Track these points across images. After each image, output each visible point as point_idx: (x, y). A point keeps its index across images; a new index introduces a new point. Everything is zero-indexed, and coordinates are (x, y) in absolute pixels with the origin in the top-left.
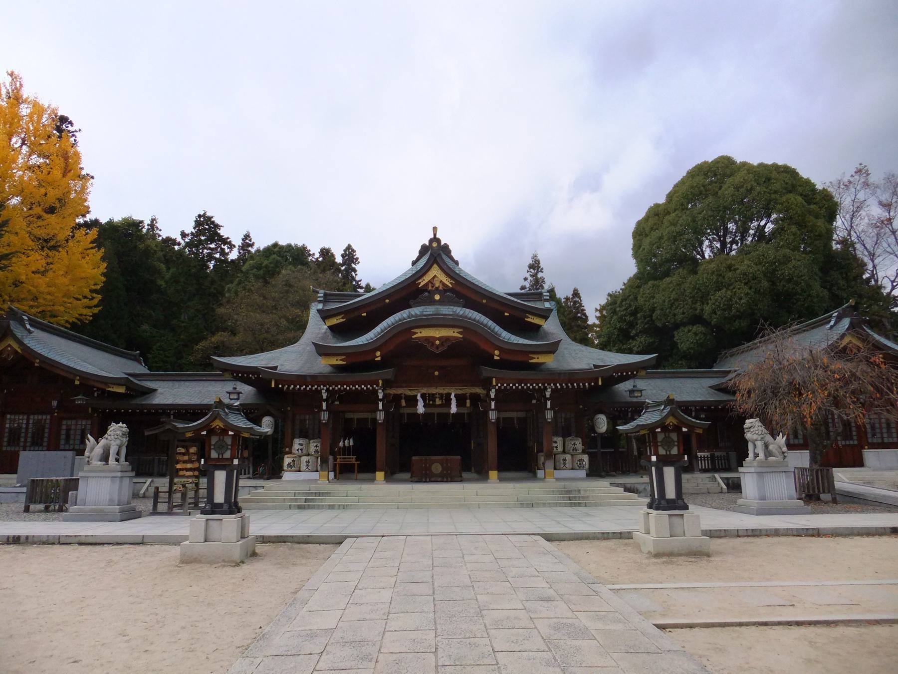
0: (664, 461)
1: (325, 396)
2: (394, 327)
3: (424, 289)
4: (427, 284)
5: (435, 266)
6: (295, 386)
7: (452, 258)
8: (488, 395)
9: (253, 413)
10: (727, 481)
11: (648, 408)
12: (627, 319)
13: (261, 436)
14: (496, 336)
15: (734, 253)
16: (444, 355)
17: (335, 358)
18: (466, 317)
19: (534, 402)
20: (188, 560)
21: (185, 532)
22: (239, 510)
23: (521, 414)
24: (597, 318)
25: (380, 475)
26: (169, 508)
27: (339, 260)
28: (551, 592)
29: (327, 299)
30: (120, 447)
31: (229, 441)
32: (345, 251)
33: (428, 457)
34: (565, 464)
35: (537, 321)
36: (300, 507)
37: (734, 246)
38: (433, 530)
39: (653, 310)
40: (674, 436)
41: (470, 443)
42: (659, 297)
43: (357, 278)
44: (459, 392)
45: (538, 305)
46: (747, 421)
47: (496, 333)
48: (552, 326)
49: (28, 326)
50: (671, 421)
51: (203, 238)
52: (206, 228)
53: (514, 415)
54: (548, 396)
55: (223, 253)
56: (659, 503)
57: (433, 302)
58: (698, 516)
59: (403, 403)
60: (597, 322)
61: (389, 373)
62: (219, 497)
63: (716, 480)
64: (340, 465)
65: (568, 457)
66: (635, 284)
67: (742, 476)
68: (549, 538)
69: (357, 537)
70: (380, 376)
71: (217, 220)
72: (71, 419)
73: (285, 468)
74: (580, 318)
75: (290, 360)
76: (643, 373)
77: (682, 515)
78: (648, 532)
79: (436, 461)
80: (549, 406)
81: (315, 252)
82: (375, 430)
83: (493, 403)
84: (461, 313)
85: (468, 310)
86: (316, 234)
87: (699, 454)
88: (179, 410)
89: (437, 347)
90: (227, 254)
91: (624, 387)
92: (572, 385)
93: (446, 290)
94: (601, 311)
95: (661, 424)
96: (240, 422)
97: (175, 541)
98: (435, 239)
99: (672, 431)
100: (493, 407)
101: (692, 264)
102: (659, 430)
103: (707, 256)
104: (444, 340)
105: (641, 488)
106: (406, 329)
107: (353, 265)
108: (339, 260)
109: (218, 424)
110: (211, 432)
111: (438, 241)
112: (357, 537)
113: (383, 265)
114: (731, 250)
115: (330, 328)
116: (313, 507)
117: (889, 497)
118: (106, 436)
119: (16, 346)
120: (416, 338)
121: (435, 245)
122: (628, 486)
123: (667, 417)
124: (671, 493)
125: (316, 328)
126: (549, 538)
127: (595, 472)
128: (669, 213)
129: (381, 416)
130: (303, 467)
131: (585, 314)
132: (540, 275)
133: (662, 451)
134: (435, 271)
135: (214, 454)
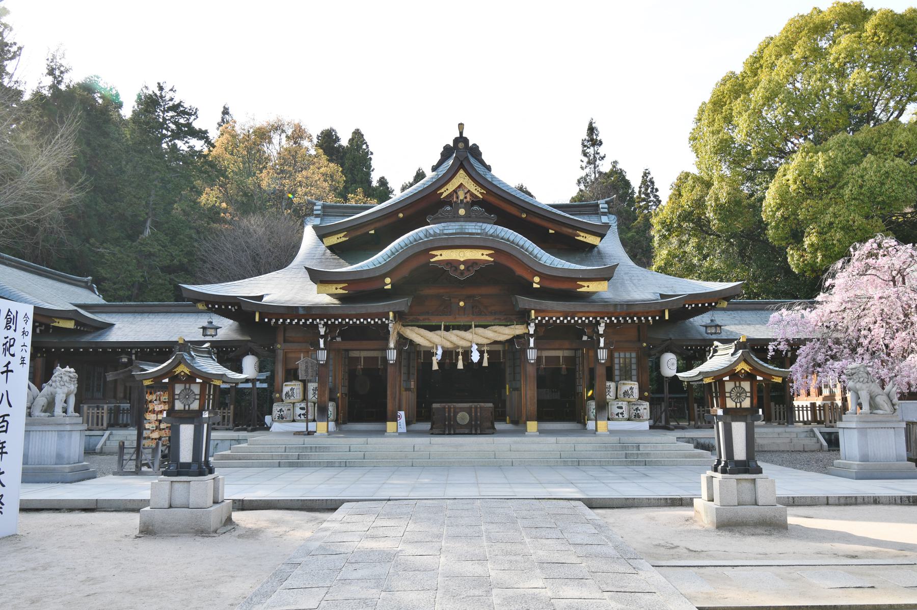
1: (322, 331)
2: (407, 247)
3: (448, 201)
4: (450, 195)
5: (461, 171)
6: (285, 320)
7: (482, 163)
9: (228, 354)
14: (535, 259)
16: (470, 282)
17: (334, 286)
18: (497, 236)
19: (585, 338)
20: (147, 531)
21: (146, 494)
22: (211, 471)
23: (567, 353)
26: (137, 466)
30: (68, 395)
31: (196, 389)
33: (452, 405)
36: (292, 465)
40: (746, 385)
41: (505, 388)
45: (593, 220)
50: (743, 367)
54: (601, 332)
56: (733, 467)
57: (456, 218)
58: (773, 482)
61: (402, 303)
62: (186, 455)
67: (840, 431)
68: (592, 504)
70: (390, 307)
75: (282, 289)
78: (711, 500)
79: (462, 409)
80: (602, 345)
82: (385, 370)
84: (491, 232)
85: (500, 228)
88: (142, 349)
89: (462, 273)
91: (700, 321)
93: (475, 202)
96: (211, 366)
97: (131, 507)
98: (461, 140)
99: (744, 380)
102: (727, 378)
104: (470, 264)
106: (425, 250)
109: (182, 369)
110: (175, 379)
111: (466, 141)
113: (401, 163)
115: (331, 248)
116: (309, 465)
117: (561, 484)
118: (50, 382)
122: (702, 441)
123: (737, 363)
124: (740, 453)
126: (592, 504)
133: (730, 404)
134: (461, 178)
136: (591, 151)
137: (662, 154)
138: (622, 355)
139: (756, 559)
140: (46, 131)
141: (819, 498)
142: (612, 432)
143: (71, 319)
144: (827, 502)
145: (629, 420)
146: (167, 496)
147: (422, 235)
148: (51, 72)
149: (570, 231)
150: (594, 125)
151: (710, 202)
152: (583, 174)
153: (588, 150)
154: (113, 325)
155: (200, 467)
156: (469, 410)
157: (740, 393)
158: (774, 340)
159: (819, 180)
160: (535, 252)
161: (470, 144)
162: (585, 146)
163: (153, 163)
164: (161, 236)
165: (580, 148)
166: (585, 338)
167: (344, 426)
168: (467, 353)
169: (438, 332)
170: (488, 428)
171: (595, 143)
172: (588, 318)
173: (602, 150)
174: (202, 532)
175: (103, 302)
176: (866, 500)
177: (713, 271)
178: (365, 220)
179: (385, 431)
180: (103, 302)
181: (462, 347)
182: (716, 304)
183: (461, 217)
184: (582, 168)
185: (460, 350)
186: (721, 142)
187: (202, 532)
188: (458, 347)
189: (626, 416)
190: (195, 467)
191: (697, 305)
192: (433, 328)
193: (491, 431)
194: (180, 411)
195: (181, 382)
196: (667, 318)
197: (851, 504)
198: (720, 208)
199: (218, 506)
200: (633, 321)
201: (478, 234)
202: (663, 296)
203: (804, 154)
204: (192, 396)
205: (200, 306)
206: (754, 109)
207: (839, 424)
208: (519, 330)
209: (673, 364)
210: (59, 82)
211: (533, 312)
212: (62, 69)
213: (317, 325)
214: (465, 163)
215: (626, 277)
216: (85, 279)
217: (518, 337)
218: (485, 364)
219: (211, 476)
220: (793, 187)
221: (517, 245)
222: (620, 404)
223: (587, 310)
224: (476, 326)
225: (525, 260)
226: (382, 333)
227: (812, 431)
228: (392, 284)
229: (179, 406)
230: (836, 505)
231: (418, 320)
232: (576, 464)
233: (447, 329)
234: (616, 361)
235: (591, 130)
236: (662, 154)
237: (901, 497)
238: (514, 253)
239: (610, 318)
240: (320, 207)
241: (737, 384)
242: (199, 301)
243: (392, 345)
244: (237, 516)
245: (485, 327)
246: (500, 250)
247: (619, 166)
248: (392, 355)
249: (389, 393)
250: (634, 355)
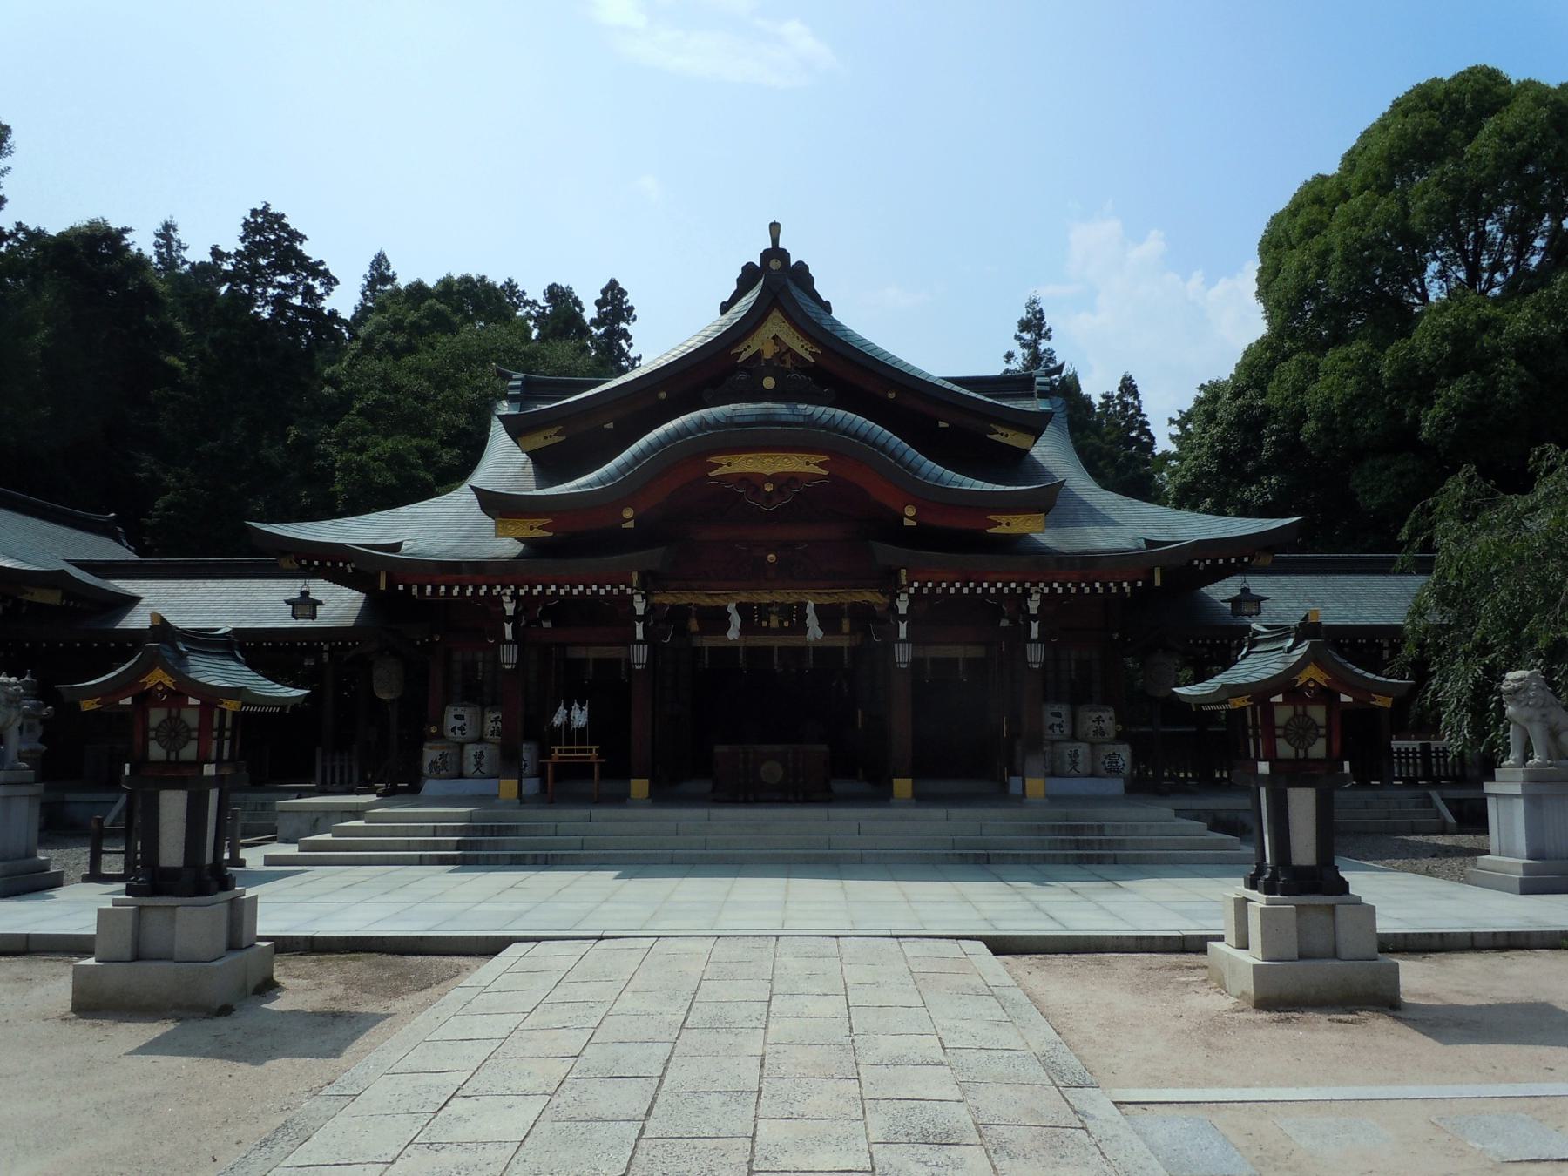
0: (1291, 773)
1: (510, 608)
5: (776, 313)
7: (815, 297)
8: (893, 608)
10: (1456, 806)
11: (1254, 643)
12: (1244, 436)
13: (283, 707)
15: (1496, 291)
19: (1004, 623)
23: (976, 652)
24: (1172, 438)
25: (639, 787)
27: (590, 313)
28: (961, 1116)
29: (530, 392)
32: (604, 292)
34: (1074, 763)
35: (1014, 439)
37: (1498, 277)
38: (728, 923)
39: (1299, 418)
40: (1318, 713)
42: (1318, 391)
43: (633, 353)
44: (826, 600)
46: (1510, 675)
47: (908, 467)
48: (1052, 453)
50: (1312, 674)
51: (263, 262)
52: (271, 240)
53: (958, 652)
55: (309, 293)
59: (694, 625)
60: (1173, 449)
63: (1429, 802)
64: (556, 766)
65: (1083, 749)
66: (1259, 366)
67: (1491, 803)
68: (1001, 946)
69: (538, 939)
71: (293, 223)
73: (426, 770)
74: (1137, 440)
76: (1266, 560)
77: (1332, 908)
78: (1243, 944)
80: (1035, 634)
81: (534, 291)
83: (903, 627)
84: (817, 414)
86: (532, 254)
87: (1395, 745)
89: (769, 496)
90: (321, 297)
91: (1222, 591)
92: (1091, 585)
94: (1182, 424)
95: (1285, 683)
98: (776, 253)
99: (1315, 701)
100: (903, 634)
101: (1394, 317)
102: (1279, 698)
103: (1432, 298)
104: (785, 481)
107: (623, 325)
108: (590, 313)
110: (145, 699)
111: (784, 255)
112: (538, 939)
114: (1491, 283)
120: (714, 478)
121: (775, 264)
125: (503, 463)
126: (1001, 946)
127: (1139, 787)
128: (1345, 196)
129: (640, 655)
130: (470, 766)
131: (1148, 433)
132: (1044, 345)
133: (1284, 749)
134: (775, 325)
142: (1053, 799)
145: (1092, 775)
146: (127, 938)
154: (139, 599)
160: (908, 457)
161: (793, 263)
166: (1004, 623)
172: (1007, 584)
175: (136, 558)
179: (627, 795)
182: (1251, 559)
191: (1215, 561)
195: (159, 704)
196: (1158, 583)
199: (238, 955)
200: (1094, 590)
202: (1150, 544)
205: (286, 563)
207: (1489, 787)
213: (499, 598)
219: (224, 896)
227: (1429, 797)
228: (636, 518)
239: (1049, 585)
240: (519, 383)
241: (1300, 709)
242: (284, 553)
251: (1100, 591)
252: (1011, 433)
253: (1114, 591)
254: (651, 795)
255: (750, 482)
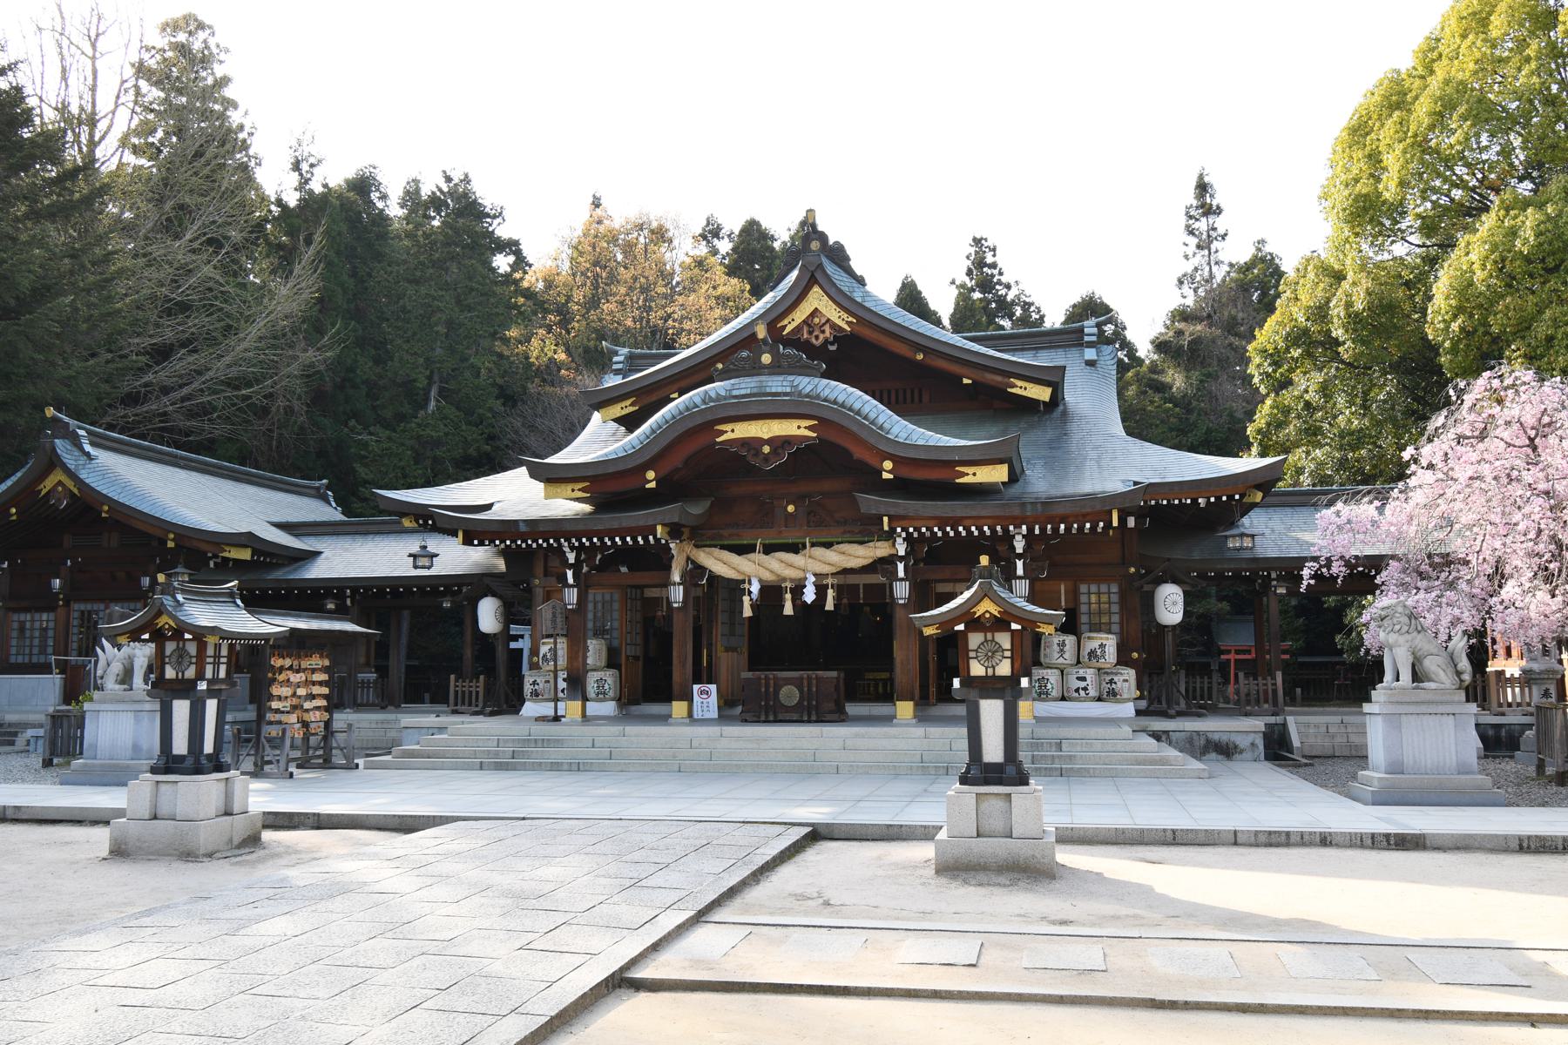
2: (675, 421)
4: (798, 329)
7: (850, 272)
13: (267, 641)
14: (880, 432)
18: (818, 397)
20: (119, 852)
25: (905, 709)
26: (255, 764)
33: (771, 675)
36: (500, 767)
49: (88, 448)
54: (1019, 550)
56: (979, 773)
57: (756, 369)
61: (672, 512)
72: (27, 610)
79: (788, 681)
84: (808, 390)
89: (766, 458)
97: (925, 833)
104: (780, 443)
105: (1243, 742)
106: (704, 425)
119: (70, 484)
122: (1216, 737)
124: (993, 751)
135: (977, 669)
136: (1202, 225)
137: (1291, 219)
138: (1094, 588)
139: (897, 919)
140: (285, 259)
141: (1219, 832)
143: (246, 546)
144: (1235, 840)
145: (1099, 699)
147: (698, 400)
148: (296, 167)
149: (999, 378)
150: (1206, 179)
151: (1337, 311)
152: (1188, 267)
153: (1197, 225)
154: (319, 553)
155: (197, 761)
156: (798, 683)
157: (993, 652)
158: (1315, 559)
159: (1528, 260)
162: (1191, 217)
163: (434, 299)
164: (451, 411)
165: (1183, 220)
167: (635, 709)
168: (798, 590)
169: (752, 556)
170: (831, 712)
171: (1209, 211)
173: (1221, 223)
174: (188, 855)
176: (1306, 837)
177: (1351, 433)
178: (661, 377)
180: (337, 516)
181: (792, 580)
182: (1242, 496)
183: (765, 367)
184: (1186, 257)
185: (788, 585)
186: (1356, 200)
187: (188, 855)
188: (784, 580)
189: (1093, 693)
190: (189, 762)
191: (1218, 498)
192: (742, 550)
193: (835, 716)
194: (170, 680)
197: (1278, 845)
198: (1354, 320)
201: (786, 394)
203: (1502, 212)
204: (186, 660)
206: (1415, 135)
208: (881, 550)
209: (1175, 603)
210: (307, 181)
211: (886, 519)
212: (312, 160)
214: (818, 276)
215: (1093, 454)
216: (317, 484)
217: (882, 560)
218: (829, 606)
220: (1480, 275)
221: (850, 409)
222: (1081, 672)
223: (974, 513)
224: (813, 545)
225: (864, 435)
226: (658, 560)
229: (170, 673)
230: (1251, 845)
231: (721, 537)
232: (943, 771)
233: (769, 549)
234: (1084, 599)
235: (1202, 188)
236: (1291, 219)
237: (1373, 836)
238: (845, 423)
243: (676, 578)
244: (267, 835)
245: (828, 545)
246: (829, 421)
247: (1268, 249)
248: (677, 594)
249: (675, 654)
250: (1114, 588)
251: (964, 534)
252: (1029, 385)
253: (964, 534)
254: (720, 716)
255: (753, 444)
